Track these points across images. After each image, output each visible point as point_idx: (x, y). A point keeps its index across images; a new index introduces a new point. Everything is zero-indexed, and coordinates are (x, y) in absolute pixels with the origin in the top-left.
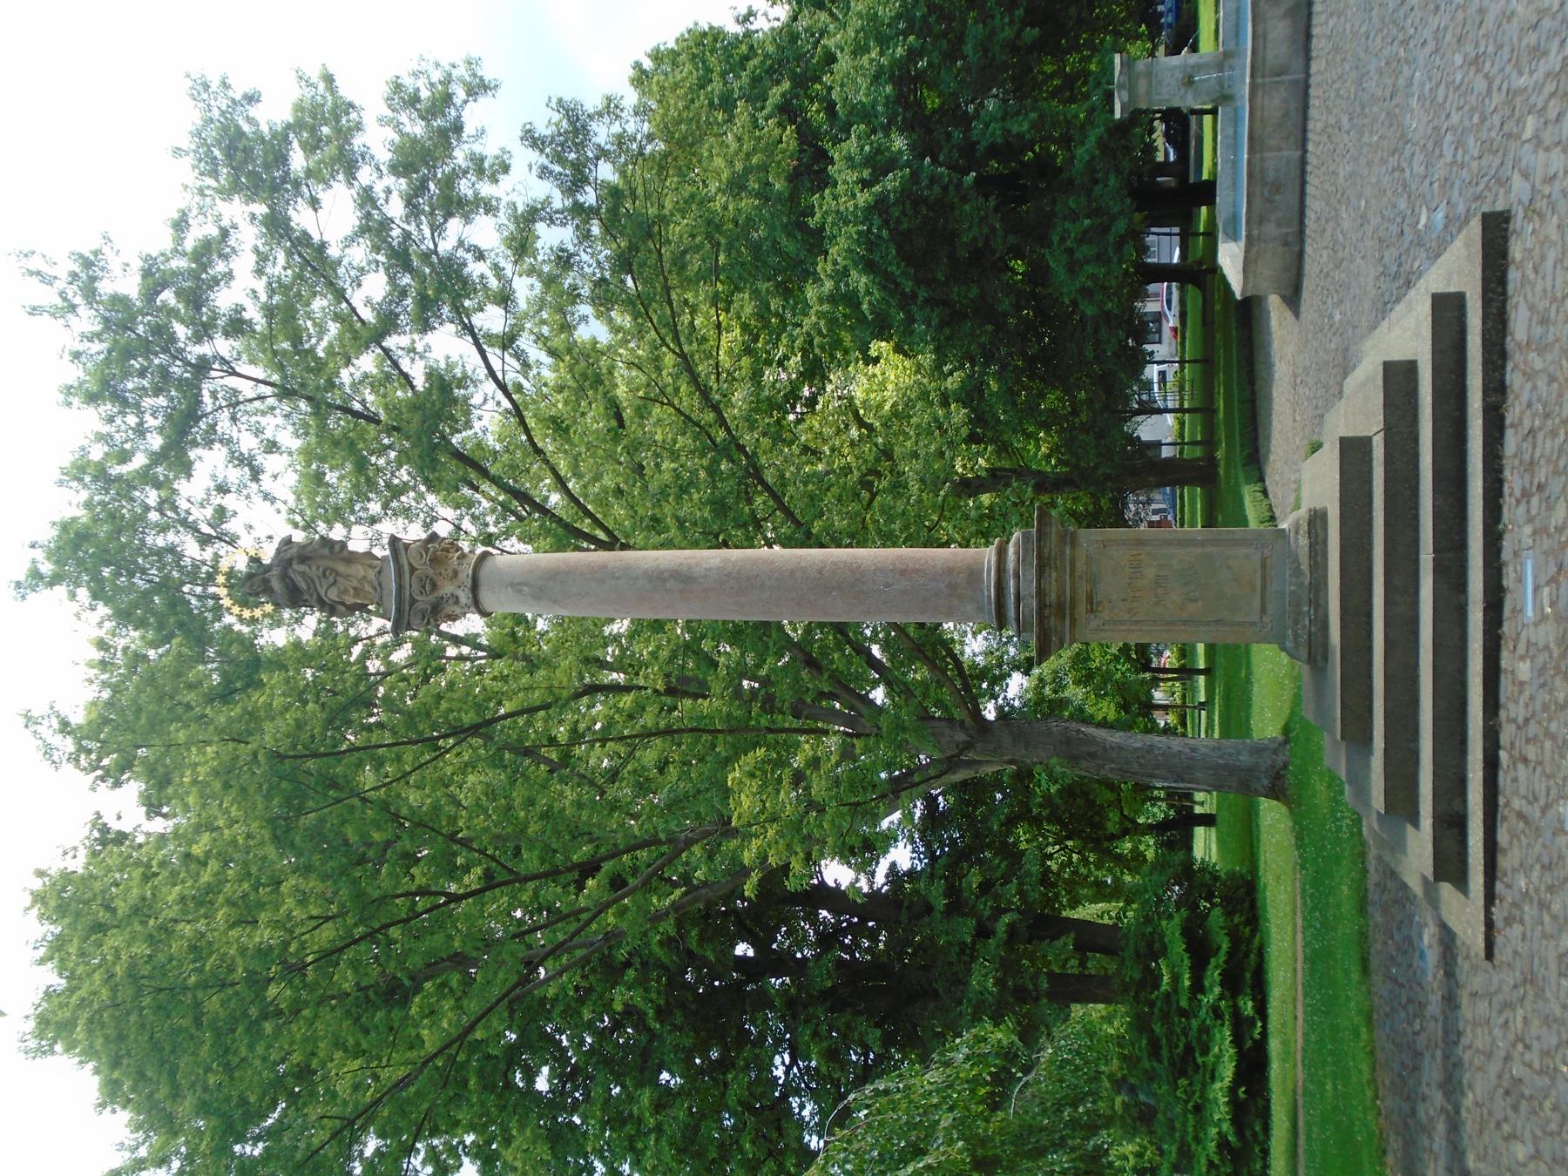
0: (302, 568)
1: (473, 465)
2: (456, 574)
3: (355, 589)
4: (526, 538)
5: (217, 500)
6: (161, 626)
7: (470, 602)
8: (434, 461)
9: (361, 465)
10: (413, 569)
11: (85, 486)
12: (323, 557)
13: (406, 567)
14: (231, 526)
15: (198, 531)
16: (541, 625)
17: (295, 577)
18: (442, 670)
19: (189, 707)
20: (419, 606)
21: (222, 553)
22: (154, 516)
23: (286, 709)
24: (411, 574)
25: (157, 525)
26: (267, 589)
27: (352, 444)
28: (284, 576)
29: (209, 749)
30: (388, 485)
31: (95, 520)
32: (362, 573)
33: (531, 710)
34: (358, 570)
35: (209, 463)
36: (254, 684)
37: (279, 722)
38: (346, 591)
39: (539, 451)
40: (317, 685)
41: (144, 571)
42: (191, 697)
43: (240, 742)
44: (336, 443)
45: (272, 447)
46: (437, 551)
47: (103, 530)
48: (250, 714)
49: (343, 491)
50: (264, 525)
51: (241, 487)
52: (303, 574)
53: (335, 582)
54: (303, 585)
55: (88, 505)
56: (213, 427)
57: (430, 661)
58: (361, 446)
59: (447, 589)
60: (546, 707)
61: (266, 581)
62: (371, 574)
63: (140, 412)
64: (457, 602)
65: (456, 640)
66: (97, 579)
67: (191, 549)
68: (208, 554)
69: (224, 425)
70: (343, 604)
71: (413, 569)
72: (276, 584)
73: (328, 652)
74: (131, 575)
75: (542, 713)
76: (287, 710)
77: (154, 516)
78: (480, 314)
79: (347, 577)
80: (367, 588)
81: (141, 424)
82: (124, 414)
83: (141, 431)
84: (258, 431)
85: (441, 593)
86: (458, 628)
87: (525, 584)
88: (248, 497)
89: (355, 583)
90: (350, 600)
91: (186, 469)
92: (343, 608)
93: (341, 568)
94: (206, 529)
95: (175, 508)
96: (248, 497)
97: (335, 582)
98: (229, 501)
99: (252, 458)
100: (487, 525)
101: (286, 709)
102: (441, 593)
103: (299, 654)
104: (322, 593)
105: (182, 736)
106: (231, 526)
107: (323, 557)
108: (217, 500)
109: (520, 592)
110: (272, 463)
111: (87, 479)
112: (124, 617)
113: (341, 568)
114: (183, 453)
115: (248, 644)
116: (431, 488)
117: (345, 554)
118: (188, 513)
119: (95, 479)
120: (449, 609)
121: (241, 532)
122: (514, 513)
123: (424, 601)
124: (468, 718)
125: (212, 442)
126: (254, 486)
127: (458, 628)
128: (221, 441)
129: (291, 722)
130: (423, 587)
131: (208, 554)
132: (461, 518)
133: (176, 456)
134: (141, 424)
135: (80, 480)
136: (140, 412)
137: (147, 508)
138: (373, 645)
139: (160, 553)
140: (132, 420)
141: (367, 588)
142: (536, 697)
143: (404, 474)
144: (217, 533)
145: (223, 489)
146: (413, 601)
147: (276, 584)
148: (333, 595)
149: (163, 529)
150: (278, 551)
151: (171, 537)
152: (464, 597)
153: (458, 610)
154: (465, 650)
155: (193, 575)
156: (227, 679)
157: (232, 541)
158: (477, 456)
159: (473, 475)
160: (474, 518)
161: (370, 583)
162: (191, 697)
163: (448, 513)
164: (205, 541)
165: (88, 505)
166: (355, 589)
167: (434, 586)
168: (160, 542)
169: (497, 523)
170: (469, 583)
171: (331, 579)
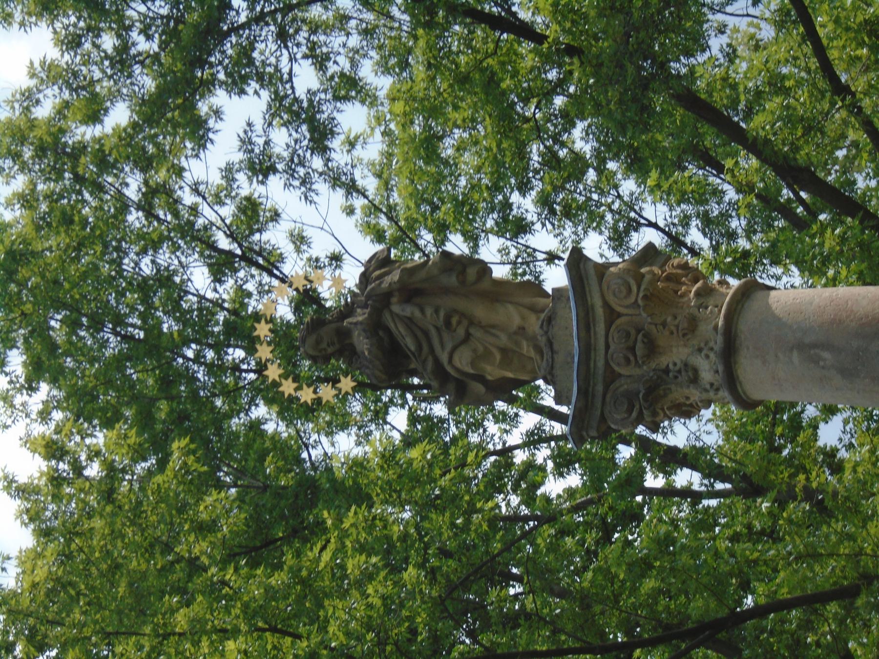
0: (409, 310)
1: (712, 123)
2: (693, 323)
3: (504, 351)
4: (814, 267)
5: (245, 186)
6: (145, 420)
7: (718, 379)
8: (646, 109)
9: (508, 123)
10: (612, 315)
11: (24, 168)
12: (447, 291)
13: (600, 311)
14: (275, 237)
15: (212, 246)
16: (830, 434)
17: (409, 327)
18: (633, 516)
19: (194, 566)
20: (623, 386)
21: (250, 286)
22: (135, 218)
23: (369, 576)
24: (609, 325)
25: (141, 236)
26: (348, 352)
27: (491, 81)
28: (376, 327)
29: (230, 645)
30: (551, 160)
31: (41, 225)
32: (517, 321)
33: (812, 601)
34: (511, 316)
35: (237, 114)
36: (306, 532)
37: (354, 600)
38: (487, 355)
39: (841, 89)
40: (419, 538)
41: (119, 321)
42: (201, 548)
43: (284, 633)
44: (462, 80)
45: (348, 87)
46: (657, 277)
47: (53, 243)
48: (303, 582)
49: (468, 170)
50: (327, 238)
51: (294, 162)
52: (409, 322)
53: (468, 336)
54: (410, 343)
55: (27, 200)
56: (246, 53)
57: (614, 502)
58: (507, 83)
59: (676, 354)
60: (845, 594)
61: (344, 335)
62: (534, 324)
63: (123, 29)
64: (695, 379)
65: (672, 459)
66: (40, 331)
67: (199, 278)
68: (227, 289)
69: (266, 48)
70: (480, 378)
71: (612, 315)
72: (362, 343)
73: (432, 479)
74: (97, 325)
75: (833, 608)
76: (371, 577)
77: (135, 218)
78: (39, 108)
79: (489, 328)
80: (526, 348)
81: (124, 48)
82: (97, 32)
83: (122, 60)
84: (320, 61)
85: (664, 361)
86: (678, 434)
87: (826, 346)
88: (305, 181)
89: (504, 340)
90: (493, 372)
91: (199, 132)
92: (480, 388)
93: (480, 311)
94: (224, 243)
95: (174, 204)
96: (305, 181)
97: (468, 336)
98: (275, 192)
99: (313, 108)
100: (732, 236)
101: (369, 576)
102: (664, 361)
103: (392, 474)
104: (444, 358)
105: (181, 620)
106: (275, 237)
107: (447, 291)
108: (245, 186)
109: (816, 361)
110: (352, 117)
111: (28, 153)
112: (84, 406)
113: (480, 311)
114: (189, 107)
115: (289, 453)
116: (637, 166)
117: (485, 285)
118: (194, 210)
119: (41, 151)
120: (679, 393)
121: (286, 247)
122: (786, 211)
123: (631, 376)
124: (699, 606)
125: (245, 79)
126: (317, 163)
127: (678, 434)
128: (260, 78)
129: (376, 601)
130: (627, 350)
131: (227, 289)
132: (685, 222)
133: (176, 111)
134: (124, 48)
135: (16, 156)
136: (123, 29)
137: (123, 206)
138: (510, 465)
139: (145, 287)
140: (108, 42)
141: (526, 348)
142: (826, 573)
143: (580, 140)
144: (245, 250)
145: (261, 167)
146: (611, 377)
147: (362, 343)
148: (463, 361)
149: (151, 244)
150: (365, 278)
151: (164, 257)
152: (708, 369)
153: (695, 395)
154: (684, 477)
155: (198, 322)
156: (257, 523)
157: (270, 263)
158: (720, 99)
159: (710, 139)
160: (708, 223)
161: (532, 340)
162: (201, 548)
163: (656, 211)
164: (221, 265)
165: (27, 200)
166: (504, 351)
167: (652, 349)
168: (146, 267)
169: (750, 232)
170: (719, 342)
171: (461, 332)
